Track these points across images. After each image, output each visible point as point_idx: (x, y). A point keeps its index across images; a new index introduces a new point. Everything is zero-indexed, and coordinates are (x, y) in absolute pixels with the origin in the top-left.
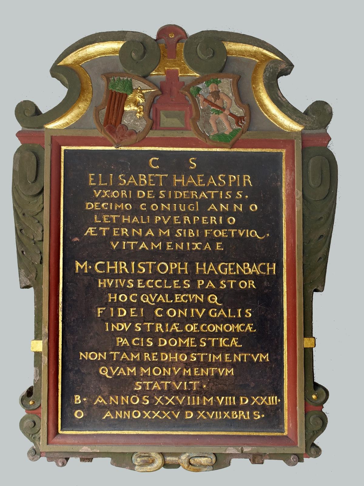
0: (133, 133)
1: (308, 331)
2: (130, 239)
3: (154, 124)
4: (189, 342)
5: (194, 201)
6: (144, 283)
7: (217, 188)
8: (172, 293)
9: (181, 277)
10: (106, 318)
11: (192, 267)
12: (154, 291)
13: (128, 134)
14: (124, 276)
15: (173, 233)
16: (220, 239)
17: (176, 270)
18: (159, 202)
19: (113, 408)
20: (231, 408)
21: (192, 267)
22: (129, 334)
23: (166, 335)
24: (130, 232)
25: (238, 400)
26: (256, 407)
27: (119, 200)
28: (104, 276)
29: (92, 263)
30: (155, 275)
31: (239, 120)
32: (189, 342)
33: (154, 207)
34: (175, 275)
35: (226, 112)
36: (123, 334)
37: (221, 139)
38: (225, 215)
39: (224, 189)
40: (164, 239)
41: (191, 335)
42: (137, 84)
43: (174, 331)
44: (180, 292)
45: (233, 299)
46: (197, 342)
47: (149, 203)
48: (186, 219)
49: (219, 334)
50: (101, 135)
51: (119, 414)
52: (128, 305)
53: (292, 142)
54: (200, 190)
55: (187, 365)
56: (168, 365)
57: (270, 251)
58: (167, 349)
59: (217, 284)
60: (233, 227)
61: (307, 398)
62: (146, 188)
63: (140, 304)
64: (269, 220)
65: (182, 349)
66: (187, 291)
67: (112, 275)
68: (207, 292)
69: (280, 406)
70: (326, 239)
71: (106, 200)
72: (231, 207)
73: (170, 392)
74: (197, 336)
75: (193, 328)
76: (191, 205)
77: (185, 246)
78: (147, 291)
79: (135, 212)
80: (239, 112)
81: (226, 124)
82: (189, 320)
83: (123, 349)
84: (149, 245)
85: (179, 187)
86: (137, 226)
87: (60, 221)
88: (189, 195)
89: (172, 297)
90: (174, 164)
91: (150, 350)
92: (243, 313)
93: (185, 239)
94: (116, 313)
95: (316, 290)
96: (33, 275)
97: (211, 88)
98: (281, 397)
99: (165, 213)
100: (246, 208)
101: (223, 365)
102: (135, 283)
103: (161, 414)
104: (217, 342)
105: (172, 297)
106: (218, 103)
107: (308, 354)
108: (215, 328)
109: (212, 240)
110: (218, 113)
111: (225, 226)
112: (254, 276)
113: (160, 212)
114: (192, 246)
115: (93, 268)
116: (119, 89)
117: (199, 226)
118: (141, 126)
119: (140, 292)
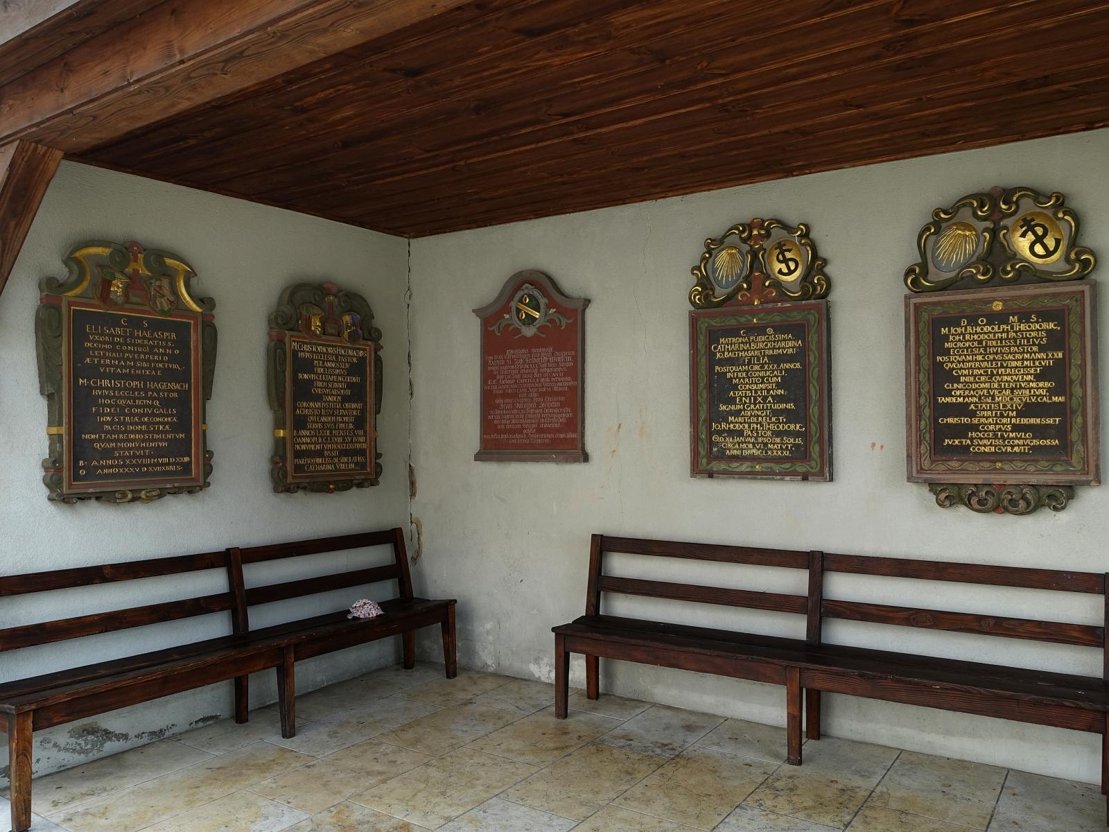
0: (116, 304)
1: (204, 422)
2: (111, 366)
3: (127, 301)
4: (144, 428)
5: (146, 346)
6: (119, 393)
7: (160, 340)
8: (135, 399)
9: (139, 390)
10: (98, 414)
11: (145, 384)
12: (125, 398)
13: (114, 304)
14: (107, 388)
15: (135, 364)
16: (160, 369)
17: (136, 386)
18: (127, 345)
19: (103, 467)
20: (166, 464)
21: (145, 384)
22: (111, 423)
23: (131, 424)
24: (111, 362)
25: (169, 460)
26: (178, 464)
27: (105, 342)
28: (97, 388)
29: (89, 380)
30: (125, 389)
31: (172, 302)
32: (144, 428)
33: (124, 348)
34: (136, 389)
35: (166, 298)
36: (107, 423)
37: (163, 312)
38: (163, 355)
39: (162, 340)
40: (130, 367)
41: (145, 423)
42: (118, 275)
43: (136, 421)
44: (139, 398)
45: (166, 403)
46: (148, 427)
47: (122, 345)
48: (142, 356)
49: (159, 423)
50: (98, 303)
51: (106, 471)
52: (110, 406)
53: (197, 318)
54: (149, 340)
55: (144, 441)
56: (132, 441)
57: (184, 377)
58: (132, 432)
59: (158, 394)
60: (166, 362)
61: (204, 456)
62: (119, 336)
63: (117, 405)
64: (184, 359)
65: (140, 432)
66: (143, 398)
67: (101, 388)
68: (155, 398)
69: (190, 462)
70: (212, 371)
71: (96, 342)
72: (165, 351)
73: (135, 456)
74: (148, 424)
75: (146, 419)
76: (825, 287)
77: (142, 372)
78: (121, 398)
79: (114, 350)
80: (172, 299)
81: (165, 305)
82: (144, 415)
83: (108, 432)
84: (122, 371)
85: (138, 337)
86: (115, 359)
87: (1043, 271)
88: (143, 342)
89: (134, 402)
90: (135, 323)
91: (123, 433)
92: (172, 411)
93: (142, 368)
94: (103, 410)
95: (208, 399)
96: (56, 386)
97: (158, 283)
98: (190, 457)
99: (130, 352)
100: (173, 352)
101: (162, 440)
102: (114, 393)
103: (129, 470)
104: (159, 428)
105: (134, 402)
106: (161, 292)
107: (204, 431)
108: (158, 419)
109: (156, 369)
110: (162, 298)
111: (162, 361)
112: (177, 391)
113: (127, 351)
114: (145, 372)
115: (90, 382)
116: (108, 277)
117: (148, 361)
118: (120, 300)
119: (117, 398)
